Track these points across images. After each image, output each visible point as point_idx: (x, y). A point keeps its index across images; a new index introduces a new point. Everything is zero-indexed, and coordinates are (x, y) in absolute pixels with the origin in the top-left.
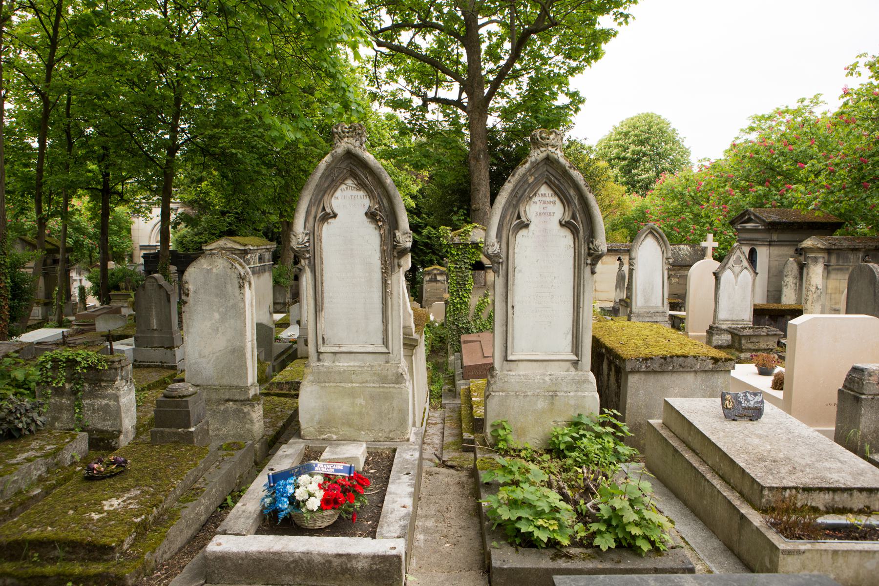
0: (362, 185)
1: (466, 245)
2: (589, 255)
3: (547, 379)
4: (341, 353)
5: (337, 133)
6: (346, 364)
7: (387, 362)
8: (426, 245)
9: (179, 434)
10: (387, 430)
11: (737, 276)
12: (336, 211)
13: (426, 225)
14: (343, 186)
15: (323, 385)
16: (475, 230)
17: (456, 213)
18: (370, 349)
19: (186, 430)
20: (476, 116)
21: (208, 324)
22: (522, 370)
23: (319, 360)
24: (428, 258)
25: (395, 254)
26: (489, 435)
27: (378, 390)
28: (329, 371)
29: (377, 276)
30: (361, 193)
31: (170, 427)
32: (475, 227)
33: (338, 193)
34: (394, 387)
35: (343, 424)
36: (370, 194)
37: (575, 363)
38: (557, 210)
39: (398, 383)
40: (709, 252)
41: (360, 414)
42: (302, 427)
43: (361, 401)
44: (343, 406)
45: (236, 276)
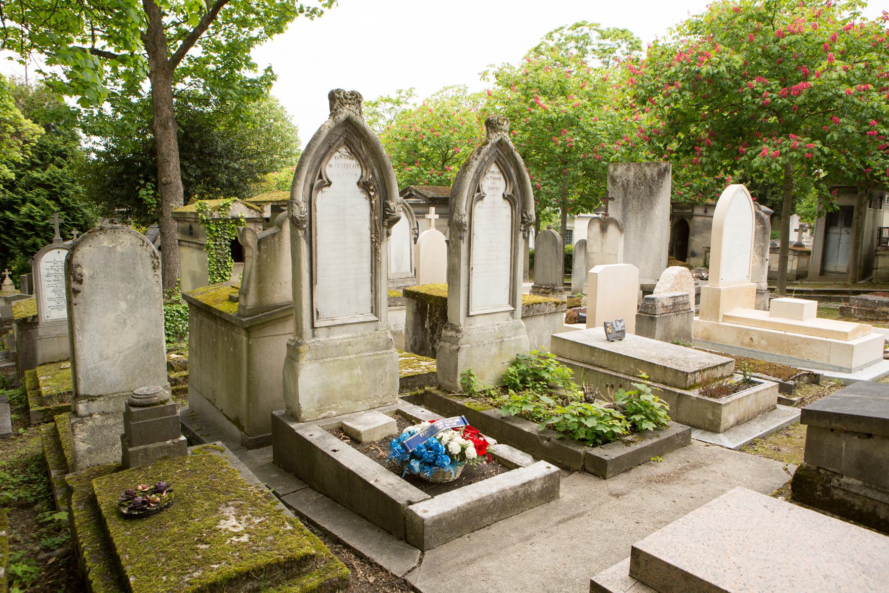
0: (354, 153)
1: (226, 220)
2: (523, 222)
3: (496, 328)
4: (335, 326)
5: (339, 98)
6: (340, 337)
7: (376, 330)
8: (26, 225)
9: (168, 447)
12: (331, 180)
13: (24, 201)
14: (337, 154)
16: (235, 204)
17: (144, 186)
18: (362, 319)
19: (176, 441)
20: (161, 78)
21: (112, 316)
22: (479, 323)
23: (314, 336)
24: (30, 241)
25: (386, 223)
26: (459, 384)
30: (354, 162)
32: (235, 201)
33: (332, 161)
35: (342, 398)
36: (363, 163)
37: (512, 312)
38: (501, 184)
39: (388, 349)
41: (358, 385)
42: (303, 409)
43: (358, 371)
44: (341, 380)
45: (148, 254)
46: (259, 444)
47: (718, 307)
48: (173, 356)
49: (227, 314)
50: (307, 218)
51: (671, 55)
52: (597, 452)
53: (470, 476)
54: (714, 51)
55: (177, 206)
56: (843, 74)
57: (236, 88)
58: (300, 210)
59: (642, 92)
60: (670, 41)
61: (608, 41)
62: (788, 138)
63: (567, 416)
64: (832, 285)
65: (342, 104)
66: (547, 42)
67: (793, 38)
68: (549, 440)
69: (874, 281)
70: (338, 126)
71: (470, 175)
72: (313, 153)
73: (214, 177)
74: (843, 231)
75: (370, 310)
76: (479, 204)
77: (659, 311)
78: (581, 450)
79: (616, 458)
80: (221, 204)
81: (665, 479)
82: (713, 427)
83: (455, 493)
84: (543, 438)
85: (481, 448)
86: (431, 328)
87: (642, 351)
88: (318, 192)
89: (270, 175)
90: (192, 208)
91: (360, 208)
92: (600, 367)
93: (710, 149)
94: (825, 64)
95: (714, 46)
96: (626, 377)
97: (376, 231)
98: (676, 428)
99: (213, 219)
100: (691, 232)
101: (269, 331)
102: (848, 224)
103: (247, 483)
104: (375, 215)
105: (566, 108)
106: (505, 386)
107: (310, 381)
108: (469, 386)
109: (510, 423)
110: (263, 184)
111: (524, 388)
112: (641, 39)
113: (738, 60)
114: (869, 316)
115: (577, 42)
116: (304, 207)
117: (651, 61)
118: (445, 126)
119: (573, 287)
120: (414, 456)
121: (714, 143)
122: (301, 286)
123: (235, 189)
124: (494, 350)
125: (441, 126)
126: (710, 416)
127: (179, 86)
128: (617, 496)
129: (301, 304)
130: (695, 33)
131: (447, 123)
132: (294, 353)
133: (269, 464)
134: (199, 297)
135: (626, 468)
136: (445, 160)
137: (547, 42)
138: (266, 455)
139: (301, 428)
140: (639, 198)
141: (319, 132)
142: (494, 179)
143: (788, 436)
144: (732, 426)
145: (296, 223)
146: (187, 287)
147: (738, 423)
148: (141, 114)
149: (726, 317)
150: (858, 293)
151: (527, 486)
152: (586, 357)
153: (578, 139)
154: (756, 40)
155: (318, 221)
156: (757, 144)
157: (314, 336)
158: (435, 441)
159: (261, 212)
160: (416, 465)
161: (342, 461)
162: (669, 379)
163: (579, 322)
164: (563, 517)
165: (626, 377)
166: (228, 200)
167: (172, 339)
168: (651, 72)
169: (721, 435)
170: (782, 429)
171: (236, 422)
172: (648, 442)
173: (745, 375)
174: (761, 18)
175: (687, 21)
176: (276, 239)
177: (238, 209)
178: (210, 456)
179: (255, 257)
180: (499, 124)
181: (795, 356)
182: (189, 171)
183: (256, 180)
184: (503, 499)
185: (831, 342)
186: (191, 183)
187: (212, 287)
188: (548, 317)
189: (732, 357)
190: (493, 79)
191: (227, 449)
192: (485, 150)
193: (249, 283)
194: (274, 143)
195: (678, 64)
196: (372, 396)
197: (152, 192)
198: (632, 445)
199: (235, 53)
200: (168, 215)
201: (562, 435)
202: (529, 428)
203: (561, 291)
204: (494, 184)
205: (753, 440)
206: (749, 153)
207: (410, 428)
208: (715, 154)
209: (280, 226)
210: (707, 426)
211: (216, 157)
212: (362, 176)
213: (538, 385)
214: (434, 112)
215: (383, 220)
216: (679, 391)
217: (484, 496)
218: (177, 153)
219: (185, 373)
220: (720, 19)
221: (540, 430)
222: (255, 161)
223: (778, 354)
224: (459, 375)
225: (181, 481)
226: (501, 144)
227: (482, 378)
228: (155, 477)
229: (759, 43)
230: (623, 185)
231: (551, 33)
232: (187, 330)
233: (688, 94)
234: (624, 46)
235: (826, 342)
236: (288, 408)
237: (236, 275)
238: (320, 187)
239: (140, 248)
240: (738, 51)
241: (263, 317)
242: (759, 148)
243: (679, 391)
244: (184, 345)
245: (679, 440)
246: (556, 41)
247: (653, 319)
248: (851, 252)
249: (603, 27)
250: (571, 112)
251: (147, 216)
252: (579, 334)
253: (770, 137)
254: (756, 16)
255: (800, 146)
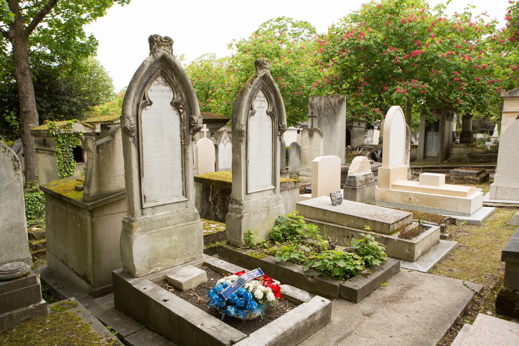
0: (168, 82)
1: (70, 135)
2: (279, 130)
3: (265, 201)
5: (156, 41)
6: (162, 214)
7: (187, 207)
9: (31, 310)
10: (192, 253)
11: (225, 146)
12: (152, 100)
14: (156, 82)
15: (149, 232)
16: (75, 124)
17: (9, 114)
18: (176, 200)
20: (19, 41)
22: (254, 198)
23: (143, 214)
25: (191, 132)
26: (243, 240)
27: (185, 227)
28: (152, 221)
29: (179, 148)
30: (168, 88)
31: (17, 308)
32: (75, 122)
33: (152, 87)
34: (194, 223)
36: (174, 89)
37: (274, 190)
38: (265, 104)
40: (205, 133)
42: (136, 269)
43: (175, 238)
44: (164, 244)
45: (10, 159)
46: (103, 293)
47: (389, 180)
48: (34, 229)
49: (75, 200)
50: (136, 128)
51: (342, 33)
52: (348, 284)
53: (270, 314)
54: (366, 32)
55: (35, 126)
56: (440, 45)
57: (72, 46)
58: (130, 123)
59: (327, 56)
60: (339, 25)
61: (297, 28)
62: (410, 81)
63: (326, 261)
64: (430, 164)
65: (159, 46)
66: (263, 28)
67: (411, 24)
68: (312, 277)
69: (451, 161)
70: (156, 62)
71: (246, 98)
72: (139, 80)
73: (59, 108)
74: (434, 134)
75: (181, 194)
76: (252, 118)
77: (358, 184)
78: (337, 283)
79: (362, 288)
80: (66, 124)
81: (394, 299)
82: (410, 258)
83: (263, 330)
84: (308, 276)
85: (276, 291)
86: (213, 201)
87: (356, 210)
88: (142, 109)
89: (96, 108)
90: (45, 127)
91: (173, 121)
92: (331, 222)
93: (366, 88)
94: (430, 40)
95: (367, 28)
96: (349, 228)
97: (185, 137)
98: (391, 263)
99: (60, 134)
100: (352, 136)
101: (107, 211)
102: (437, 130)
103: (99, 336)
104: (184, 126)
105: (281, 65)
106: (273, 239)
107: (141, 248)
108: (249, 242)
109: (283, 266)
110: (93, 112)
111: (285, 240)
112: (316, 27)
113: (380, 36)
114: (460, 181)
115: (280, 29)
116: (133, 120)
117: (331, 38)
118: (207, 76)
119: (289, 170)
120: (229, 303)
121: (368, 85)
122: (132, 178)
123: (71, 115)
124: (264, 216)
125: (204, 76)
126: (407, 251)
127: (33, 48)
128: (368, 315)
129: (132, 192)
130: (355, 21)
131: (208, 74)
132: (128, 228)
133: (112, 309)
134: (52, 188)
135: (367, 293)
136: (207, 97)
137: (263, 28)
138: (108, 302)
139: (137, 283)
140: (327, 116)
141: (143, 65)
142: (261, 101)
143: (453, 260)
144: (420, 257)
145: (126, 132)
146: (43, 181)
147: (423, 254)
148: (6, 67)
149: (394, 186)
150: (452, 168)
151: (312, 318)
152: (321, 216)
153: (288, 83)
154: (390, 25)
155: (143, 131)
156: (393, 85)
157: (143, 214)
158: (244, 290)
159: (94, 129)
160: (232, 310)
161: (172, 309)
162: (381, 228)
163: (306, 193)
164: (338, 337)
165: (349, 228)
166: (70, 121)
167: (33, 217)
168: (332, 43)
169: (415, 263)
170: (447, 256)
171: (85, 277)
172: (378, 274)
173: (419, 222)
174: (392, 12)
175: (350, 15)
176: (110, 145)
177: (78, 127)
178: (66, 314)
179: (95, 158)
180: (264, 64)
181: (437, 208)
182: (42, 104)
183: (88, 110)
184: (298, 330)
185: (457, 199)
186: (43, 112)
187: (62, 181)
188: (290, 191)
189: (410, 211)
190: (235, 47)
191: (80, 304)
192: (255, 81)
193: (91, 177)
194: (98, 89)
195: (346, 39)
196: (185, 254)
197: (15, 118)
198: (369, 276)
199: (72, 29)
200: (28, 132)
201: (321, 273)
202: (297, 269)
203: (285, 174)
204: (261, 104)
205: (434, 265)
206: (389, 90)
207: (222, 280)
208: (369, 91)
209: (113, 135)
210: (405, 258)
211: (60, 95)
212: (174, 98)
213: (295, 238)
214: (199, 67)
215: (189, 130)
216: (385, 236)
217: (286, 330)
218: (33, 92)
219: (43, 241)
220: (370, 12)
221: (305, 270)
222: (87, 98)
223: (426, 206)
224: (242, 234)
225: (43, 340)
226: (265, 77)
227: (257, 235)
228: (19, 339)
229: (392, 27)
230: (318, 109)
231: (265, 23)
232: (44, 210)
233: (353, 57)
234: (306, 31)
235: (455, 199)
236: (125, 267)
237: (78, 172)
238: (144, 106)
239: (2, 154)
240: (380, 31)
241: (103, 202)
242: (395, 88)
243: (385, 236)
244: (42, 220)
245: (394, 270)
246: (268, 28)
247: (355, 189)
248: (439, 145)
249: (294, 21)
250: (283, 67)
251: (13, 133)
252: (309, 201)
253: (401, 81)
254: (389, 11)
255: (418, 86)
